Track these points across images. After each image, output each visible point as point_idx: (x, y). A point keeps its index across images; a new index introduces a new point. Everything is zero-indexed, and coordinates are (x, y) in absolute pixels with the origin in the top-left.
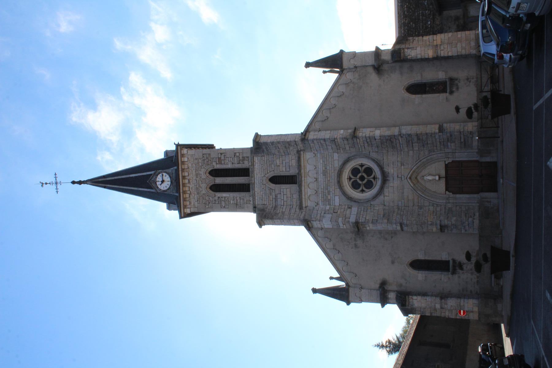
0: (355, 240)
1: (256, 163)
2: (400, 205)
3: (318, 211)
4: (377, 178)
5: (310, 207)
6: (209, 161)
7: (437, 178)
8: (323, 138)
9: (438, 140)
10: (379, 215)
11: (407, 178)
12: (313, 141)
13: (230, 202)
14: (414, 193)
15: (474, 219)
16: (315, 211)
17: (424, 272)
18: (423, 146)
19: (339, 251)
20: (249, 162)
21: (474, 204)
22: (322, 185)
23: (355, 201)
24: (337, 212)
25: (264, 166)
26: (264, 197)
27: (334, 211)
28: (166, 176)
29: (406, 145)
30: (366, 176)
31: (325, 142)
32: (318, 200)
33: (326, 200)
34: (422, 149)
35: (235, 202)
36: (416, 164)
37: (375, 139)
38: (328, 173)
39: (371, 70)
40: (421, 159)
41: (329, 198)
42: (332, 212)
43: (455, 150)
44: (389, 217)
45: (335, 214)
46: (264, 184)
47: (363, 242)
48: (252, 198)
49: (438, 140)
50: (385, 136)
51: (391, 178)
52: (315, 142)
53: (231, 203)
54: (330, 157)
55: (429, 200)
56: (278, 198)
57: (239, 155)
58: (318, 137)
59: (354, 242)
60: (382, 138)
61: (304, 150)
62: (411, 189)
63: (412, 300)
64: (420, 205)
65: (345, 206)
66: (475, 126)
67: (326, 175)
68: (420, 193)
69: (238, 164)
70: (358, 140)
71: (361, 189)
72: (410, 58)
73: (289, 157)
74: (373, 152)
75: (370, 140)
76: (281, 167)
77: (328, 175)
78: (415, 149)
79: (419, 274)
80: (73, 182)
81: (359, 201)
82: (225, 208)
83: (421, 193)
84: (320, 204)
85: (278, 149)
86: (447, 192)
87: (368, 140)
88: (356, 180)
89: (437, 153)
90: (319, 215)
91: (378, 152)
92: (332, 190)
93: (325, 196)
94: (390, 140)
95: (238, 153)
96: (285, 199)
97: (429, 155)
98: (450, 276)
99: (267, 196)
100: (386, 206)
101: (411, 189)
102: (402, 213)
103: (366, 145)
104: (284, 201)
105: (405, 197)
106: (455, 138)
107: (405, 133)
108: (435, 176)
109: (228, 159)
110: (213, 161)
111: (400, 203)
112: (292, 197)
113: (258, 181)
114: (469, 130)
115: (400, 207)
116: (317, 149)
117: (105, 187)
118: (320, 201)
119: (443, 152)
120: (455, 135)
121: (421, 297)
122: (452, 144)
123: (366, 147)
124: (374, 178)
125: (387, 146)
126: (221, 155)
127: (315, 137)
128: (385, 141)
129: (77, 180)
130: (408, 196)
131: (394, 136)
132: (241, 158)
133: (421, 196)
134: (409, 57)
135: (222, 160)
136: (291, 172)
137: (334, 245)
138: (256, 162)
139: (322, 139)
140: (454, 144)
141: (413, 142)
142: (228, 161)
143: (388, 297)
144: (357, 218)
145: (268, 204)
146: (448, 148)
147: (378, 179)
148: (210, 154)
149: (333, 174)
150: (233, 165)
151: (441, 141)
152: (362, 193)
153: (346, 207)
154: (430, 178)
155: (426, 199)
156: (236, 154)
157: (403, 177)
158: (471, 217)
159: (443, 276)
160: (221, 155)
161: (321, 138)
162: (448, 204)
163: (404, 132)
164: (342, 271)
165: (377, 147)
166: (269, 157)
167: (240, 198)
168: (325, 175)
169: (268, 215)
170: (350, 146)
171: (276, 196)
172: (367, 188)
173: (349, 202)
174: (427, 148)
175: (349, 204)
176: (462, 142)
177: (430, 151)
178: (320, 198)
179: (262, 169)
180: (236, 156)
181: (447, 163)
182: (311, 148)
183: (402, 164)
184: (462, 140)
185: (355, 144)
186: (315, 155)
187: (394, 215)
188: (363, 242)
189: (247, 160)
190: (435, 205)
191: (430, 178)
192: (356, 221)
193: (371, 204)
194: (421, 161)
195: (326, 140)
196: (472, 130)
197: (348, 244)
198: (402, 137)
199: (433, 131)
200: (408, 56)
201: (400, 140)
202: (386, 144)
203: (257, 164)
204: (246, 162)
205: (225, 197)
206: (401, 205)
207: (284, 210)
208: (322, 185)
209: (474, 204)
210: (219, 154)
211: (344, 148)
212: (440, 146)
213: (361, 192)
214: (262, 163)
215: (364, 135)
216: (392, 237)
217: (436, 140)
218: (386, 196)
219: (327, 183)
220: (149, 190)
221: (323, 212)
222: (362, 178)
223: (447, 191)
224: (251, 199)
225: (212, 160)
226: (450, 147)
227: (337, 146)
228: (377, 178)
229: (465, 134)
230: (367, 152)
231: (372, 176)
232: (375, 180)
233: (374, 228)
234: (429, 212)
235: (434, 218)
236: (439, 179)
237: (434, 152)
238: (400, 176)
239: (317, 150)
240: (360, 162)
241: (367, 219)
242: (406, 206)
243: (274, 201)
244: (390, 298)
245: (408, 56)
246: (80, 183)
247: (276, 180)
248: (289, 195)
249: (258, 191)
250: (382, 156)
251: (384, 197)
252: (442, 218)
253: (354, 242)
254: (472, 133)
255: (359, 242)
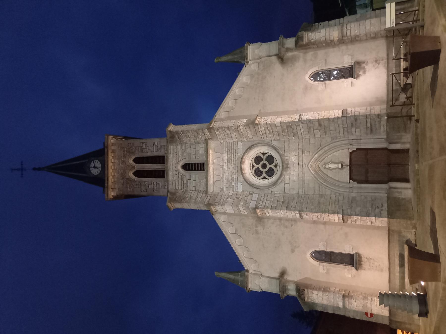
0: (256, 227)
1: (171, 151)
2: (300, 193)
3: (222, 196)
4: (278, 166)
5: (215, 192)
6: (133, 150)
7: (340, 166)
8: (227, 126)
9: (341, 126)
10: (278, 202)
11: (308, 166)
12: (218, 130)
13: (148, 186)
14: (315, 181)
15: (382, 210)
16: (219, 197)
17: (325, 264)
18: (325, 132)
19: (240, 236)
20: (165, 151)
21: (381, 195)
22: (227, 172)
23: (256, 188)
24: (238, 198)
25: (177, 154)
26: (176, 183)
27: (237, 197)
28: (98, 162)
29: (307, 133)
30: (267, 164)
31: (229, 130)
32: (223, 186)
33: (230, 186)
34: (325, 136)
35: (153, 187)
36: (318, 152)
37: (276, 126)
38: (233, 160)
39: (274, 59)
40: (322, 147)
41: (233, 184)
42: (235, 197)
43: (361, 136)
44: (288, 204)
45: (237, 199)
46: (177, 170)
47: (264, 229)
48: (166, 183)
49: (341, 126)
50: (285, 123)
51: (291, 166)
52: (220, 130)
53: (149, 187)
54: (235, 145)
55: (331, 188)
56: (188, 183)
57: (157, 144)
58: (223, 126)
59: (255, 228)
60: (282, 125)
61: (211, 139)
62: (312, 177)
63: (312, 294)
64: (321, 193)
65: (247, 192)
66: (384, 109)
67: (231, 162)
68: (321, 181)
69: (156, 152)
70: (259, 127)
71: (262, 176)
72: (313, 41)
73: (199, 145)
74: (275, 140)
75: (271, 127)
76: (191, 155)
77: (233, 162)
78: (316, 136)
79: (320, 266)
80: (34, 169)
81: (260, 188)
82: (144, 192)
83: (323, 181)
84: (225, 190)
85: (189, 138)
86: (351, 181)
87: (269, 128)
88: (259, 168)
89: (340, 139)
90: (222, 200)
91: (279, 140)
92: (236, 177)
93: (229, 182)
94: (291, 127)
95: (157, 142)
96: (194, 185)
97: (332, 142)
98: (355, 271)
99: (179, 182)
100: (286, 194)
101: (312, 177)
102: (302, 201)
103: (268, 132)
104: (193, 186)
105: (305, 184)
106: (360, 123)
107: (305, 119)
108: (338, 163)
109: (148, 148)
110: (136, 149)
111: (300, 191)
112: (200, 183)
113: (172, 168)
114: (377, 113)
115: (301, 195)
116: (223, 138)
117: (57, 173)
118: (225, 186)
119: (347, 139)
120: (360, 119)
121: (322, 293)
122: (357, 130)
123: (267, 134)
124: (276, 166)
125: (288, 133)
126: (143, 144)
127: (220, 126)
128: (286, 128)
129: (37, 167)
130: (308, 184)
131: (295, 122)
132: (159, 147)
133: (323, 184)
134: (312, 40)
135: (143, 148)
136: (200, 159)
137: (236, 230)
138: (171, 150)
139: (225, 127)
140: (359, 130)
141: (314, 129)
142: (148, 149)
143: (288, 288)
144: (257, 204)
145: (179, 189)
146: (352, 134)
147: (279, 167)
148: (133, 143)
149: (237, 162)
150: (152, 153)
151: (344, 127)
152: (264, 180)
153: (248, 193)
154: (332, 166)
155: (327, 188)
156: (155, 143)
157: (304, 164)
158: (378, 207)
159: (346, 270)
160: (143, 144)
161: (225, 126)
162: (352, 193)
163: (304, 117)
164: (243, 256)
165: (279, 134)
166: (182, 145)
167: (156, 183)
168: (230, 163)
169: (178, 199)
170: (252, 135)
171: (187, 182)
172: (268, 175)
173: (249, 189)
174: (330, 135)
175: (250, 190)
176: (369, 127)
177: (332, 138)
178: (225, 184)
179: (176, 157)
180: (154, 145)
181: (351, 151)
182: (217, 137)
183: (303, 152)
184: (369, 125)
185: (257, 132)
186: (222, 144)
187: (294, 202)
188: (264, 229)
189: (164, 148)
190: (338, 194)
191: (332, 166)
192: (256, 207)
193: (272, 191)
194: (322, 148)
195: (230, 128)
196: (379, 113)
197: (249, 229)
198: (302, 123)
199: (336, 115)
200: (311, 40)
201: (301, 127)
202: (287, 131)
203: (171, 152)
204: (162, 150)
205: (144, 182)
206: (301, 193)
207: (192, 195)
208: (227, 172)
209: (381, 195)
210: (141, 143)
211: (247, 136)
212: (343, 133)
213: (263, 179)
214: (176, 152)
215: (265, 122)
216: (292, 225)
217: (339, 125)
218: (287, 183)
219: (231, 170)
220: (84, 175)
221: (226, 197)
222: (264, 166)
223: (350, 180)
224: (166, 184)
225: (135, 148)
226: (354, 133)
227: (240, 135)
228: (278, 166)
229: (371, 118)
230: (268, 140)
231: (274, 164)
232: (276, 167)
233: (274, 215)
234: (331, 200)
235: (336, 207)
236: (342, 167)
237: (337, 139)
238: (301, 163)
239: (222, 139)
240: (262, 151)
241: (266, 205)
242: (307, 194)
243: (185, 186)
244: (290, 289)
245: (311, 40)
246: (39, 169)
247: (187, 167)
248: (198, 181)
249: (172, 177)
250: (283, 144)
251: (284, 184)
252: (344, 208)
253: (255, 228)
254: (380, 117)
255: (260, 229)
